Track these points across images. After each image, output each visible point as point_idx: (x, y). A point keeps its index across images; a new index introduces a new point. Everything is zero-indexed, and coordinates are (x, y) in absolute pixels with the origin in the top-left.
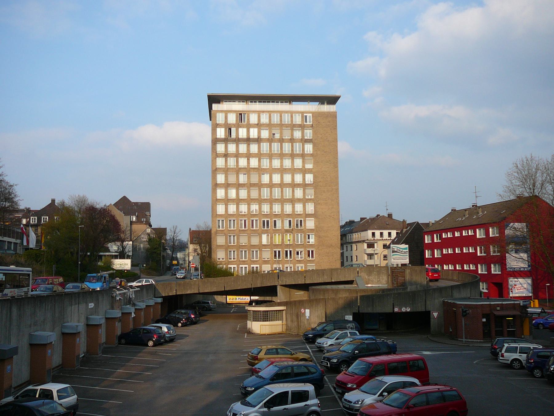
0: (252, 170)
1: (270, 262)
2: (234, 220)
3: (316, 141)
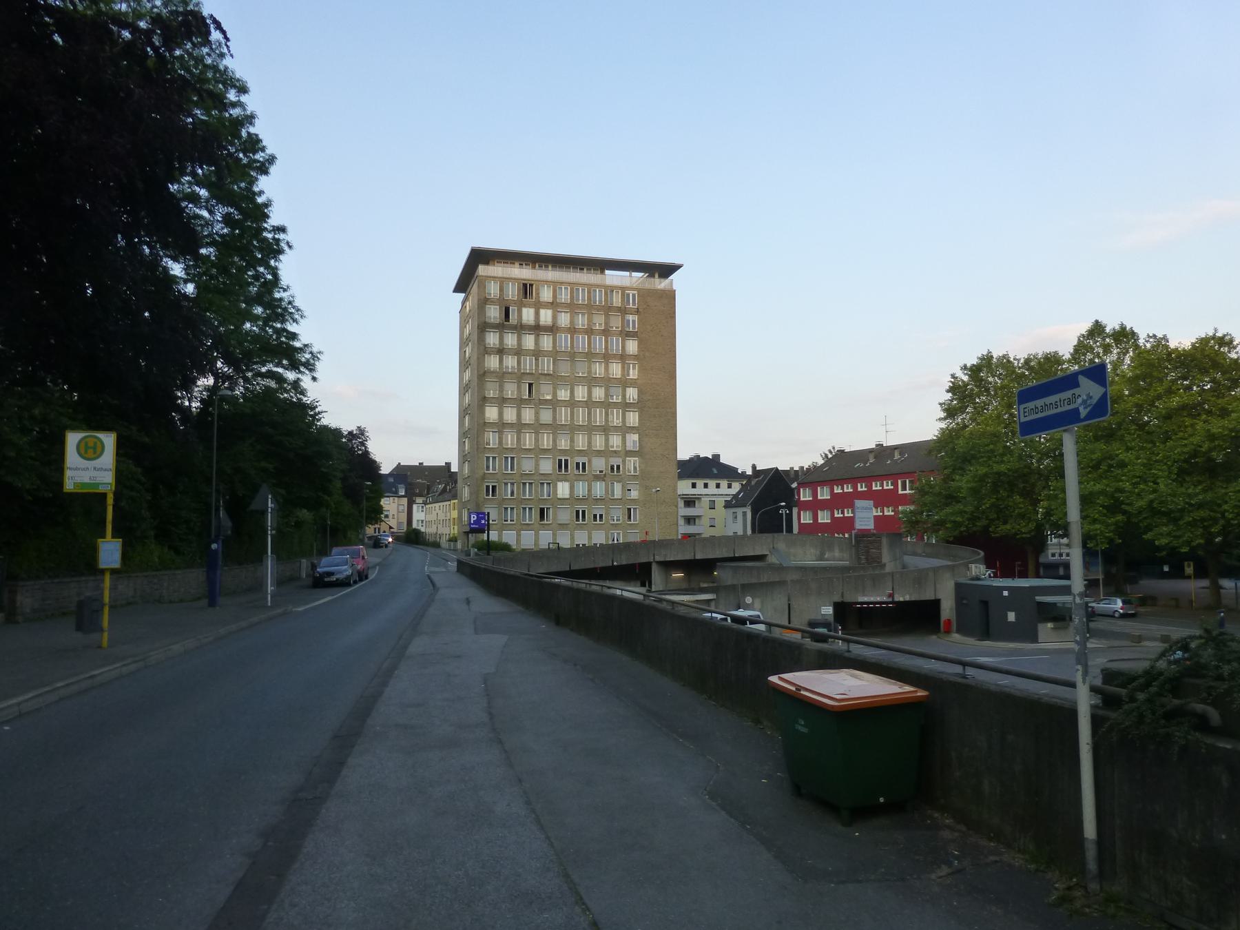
2: (512, 458)
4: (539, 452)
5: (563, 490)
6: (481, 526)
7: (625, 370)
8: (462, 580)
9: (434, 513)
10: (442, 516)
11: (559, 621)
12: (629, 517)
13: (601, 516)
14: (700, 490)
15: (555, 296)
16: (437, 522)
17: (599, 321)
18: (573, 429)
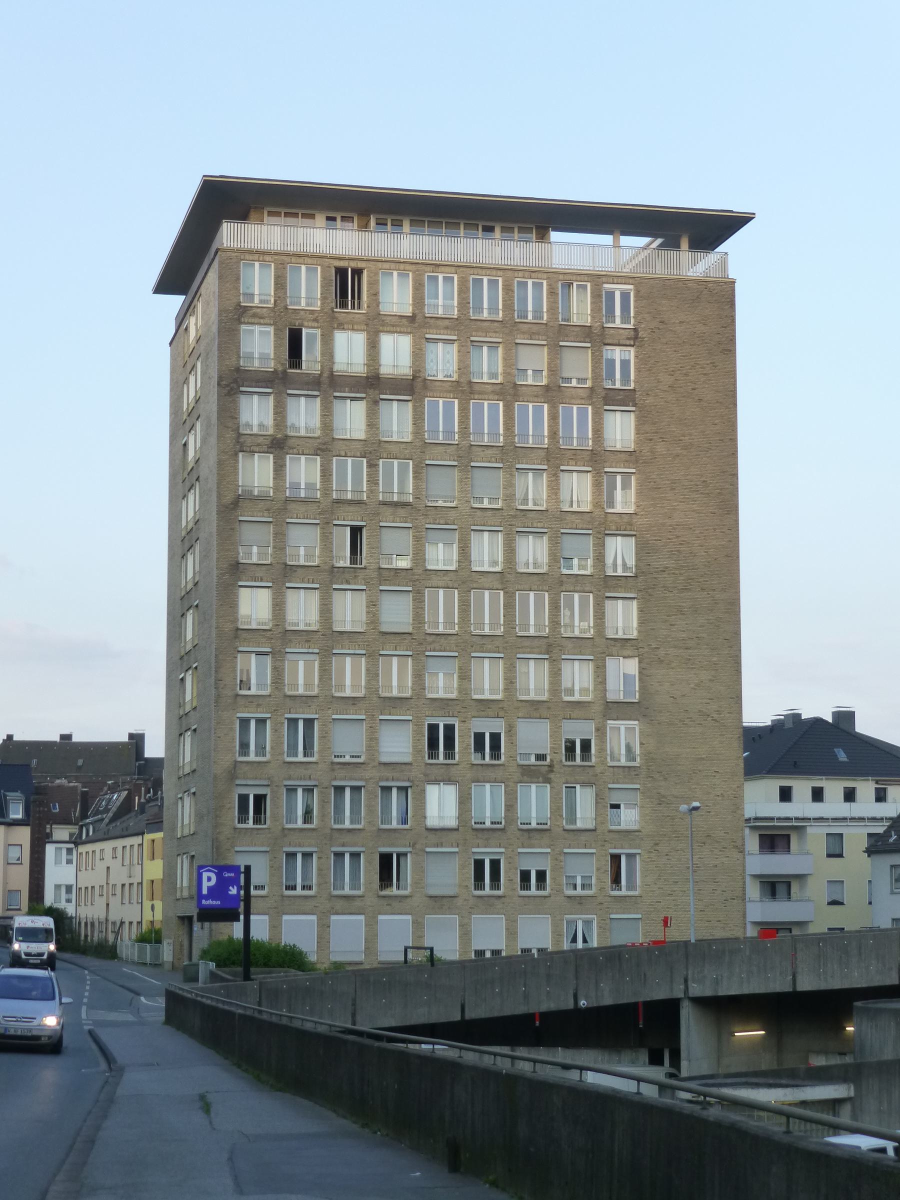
0: (388, 511)
1: (459, 902)
2: (309, 723)
3: (650, 400)
4: (378, 706)
5: (440, 805)
6: (226, 901)
7: (603, 491)
8: (179, 1044)
9: (101, 867)
10: (119, 876)
11: (457, 1159)
12: (616, 880)
13: (541, 875)
14: (802, 806)
15: (419, 300)
16: (108, 890)
17: (534, 364)
18: (466, 646)
